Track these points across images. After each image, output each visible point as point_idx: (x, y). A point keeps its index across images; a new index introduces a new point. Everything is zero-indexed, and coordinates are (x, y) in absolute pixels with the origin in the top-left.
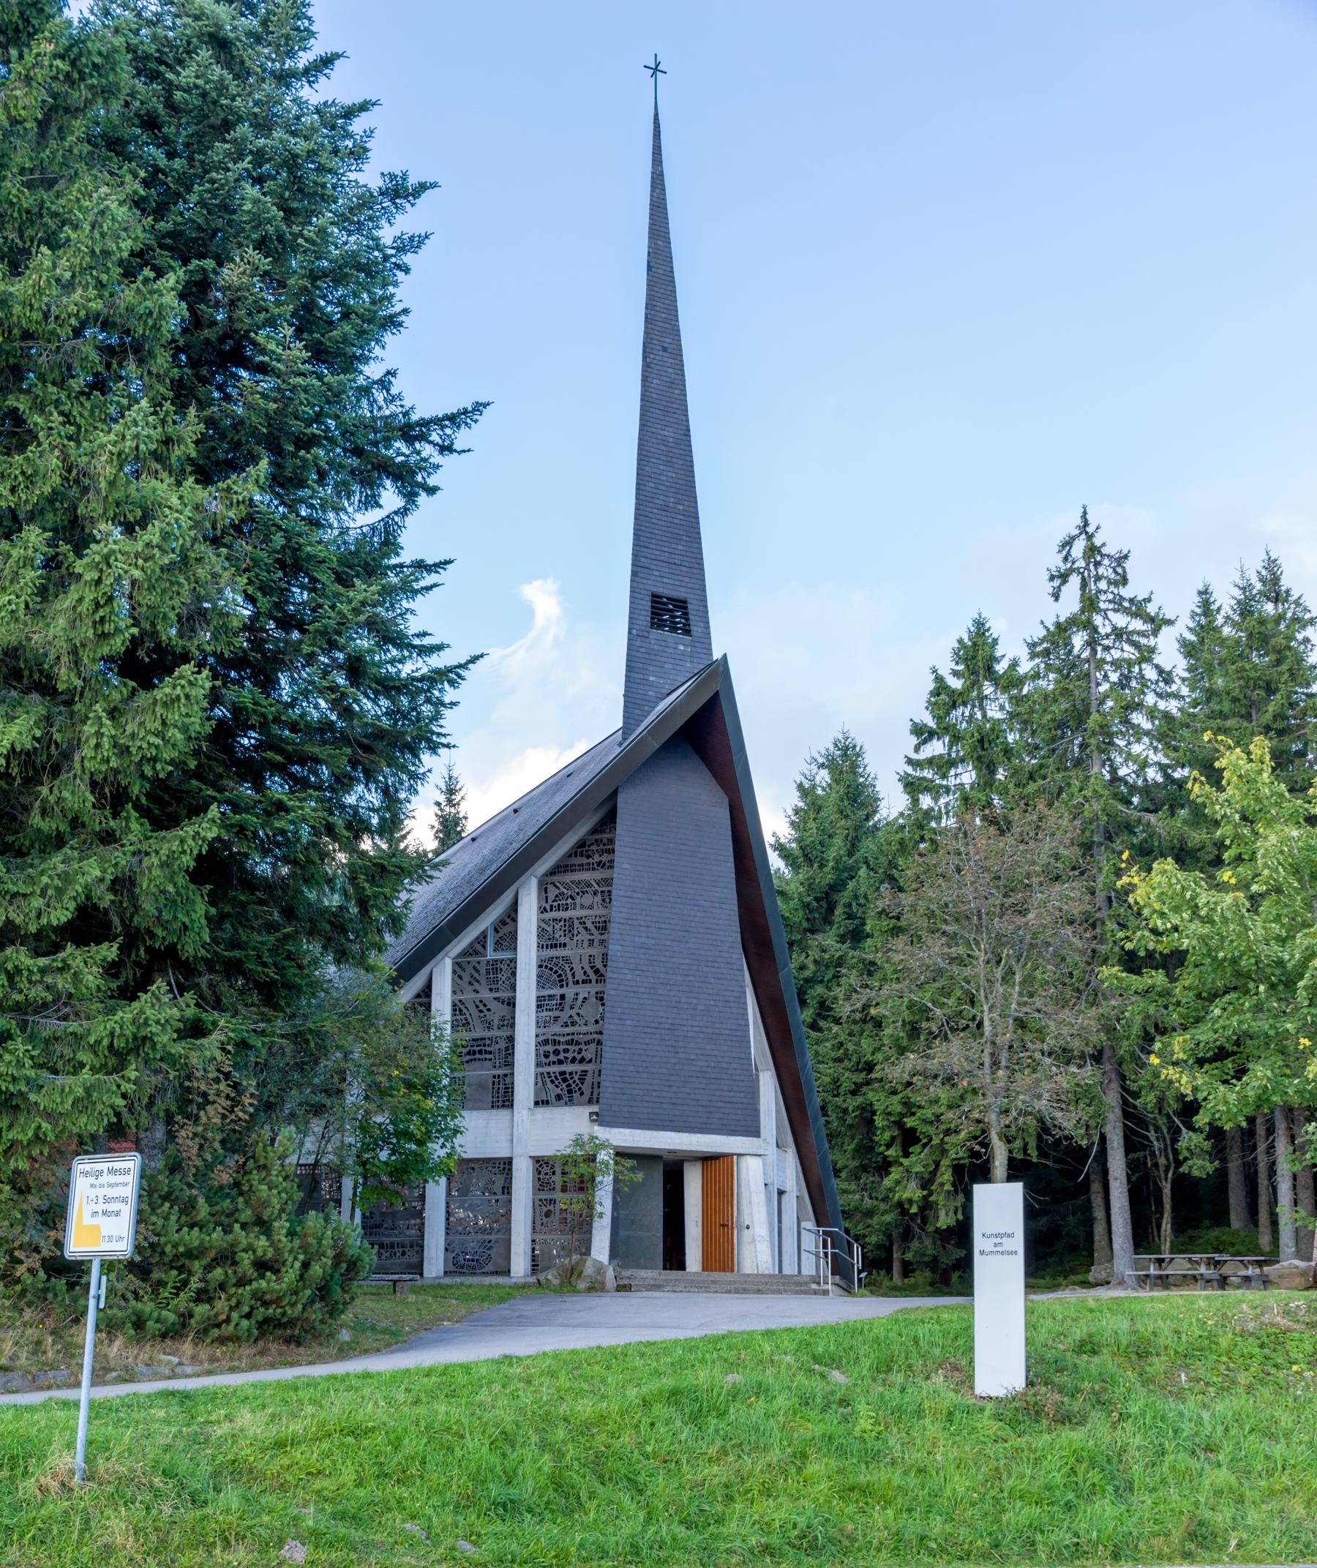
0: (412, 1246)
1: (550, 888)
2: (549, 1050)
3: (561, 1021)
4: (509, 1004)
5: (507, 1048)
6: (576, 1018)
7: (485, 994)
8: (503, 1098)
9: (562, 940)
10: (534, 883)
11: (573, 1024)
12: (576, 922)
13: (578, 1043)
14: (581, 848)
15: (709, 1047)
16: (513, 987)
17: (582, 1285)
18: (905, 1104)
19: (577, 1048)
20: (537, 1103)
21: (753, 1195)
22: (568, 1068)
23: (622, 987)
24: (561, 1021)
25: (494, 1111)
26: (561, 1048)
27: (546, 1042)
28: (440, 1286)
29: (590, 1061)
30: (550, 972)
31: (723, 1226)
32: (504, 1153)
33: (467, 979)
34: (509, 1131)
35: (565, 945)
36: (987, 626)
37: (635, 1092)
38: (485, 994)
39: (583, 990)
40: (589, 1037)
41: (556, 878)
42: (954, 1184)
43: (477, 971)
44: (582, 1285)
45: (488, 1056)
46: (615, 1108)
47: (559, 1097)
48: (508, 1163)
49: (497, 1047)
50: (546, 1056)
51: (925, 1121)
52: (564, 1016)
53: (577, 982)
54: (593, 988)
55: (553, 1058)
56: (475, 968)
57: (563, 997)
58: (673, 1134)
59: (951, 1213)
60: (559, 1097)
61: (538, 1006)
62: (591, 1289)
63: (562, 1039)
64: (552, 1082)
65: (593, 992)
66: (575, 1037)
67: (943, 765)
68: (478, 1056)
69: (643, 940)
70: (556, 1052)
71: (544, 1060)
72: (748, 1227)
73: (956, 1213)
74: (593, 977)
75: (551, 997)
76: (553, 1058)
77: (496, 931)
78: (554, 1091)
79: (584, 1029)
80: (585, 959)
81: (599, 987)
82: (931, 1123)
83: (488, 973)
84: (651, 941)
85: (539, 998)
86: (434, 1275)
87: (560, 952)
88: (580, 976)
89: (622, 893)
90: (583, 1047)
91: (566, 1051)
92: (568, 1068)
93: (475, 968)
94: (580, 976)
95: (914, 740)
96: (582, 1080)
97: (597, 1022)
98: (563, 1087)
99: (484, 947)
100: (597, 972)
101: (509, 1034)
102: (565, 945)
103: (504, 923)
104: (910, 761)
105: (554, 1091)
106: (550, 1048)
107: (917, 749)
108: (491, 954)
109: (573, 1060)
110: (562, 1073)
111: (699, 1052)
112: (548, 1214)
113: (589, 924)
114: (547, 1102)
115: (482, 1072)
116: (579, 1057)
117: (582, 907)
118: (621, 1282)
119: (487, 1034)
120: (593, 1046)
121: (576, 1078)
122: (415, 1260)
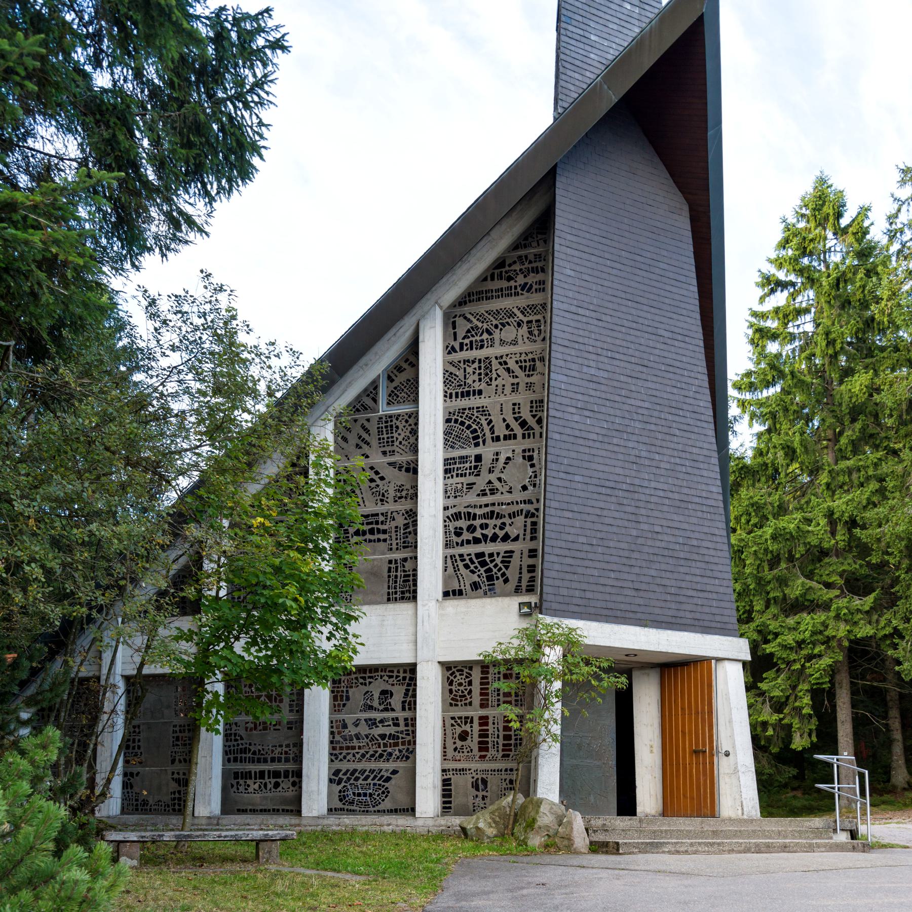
0: (286, 776)
1: (460, 321)
2: (460, 526)
3: (477, 489)
4: (407, 470)
5: (406, 526)
6: (497, 484)
7: (377, 459)
8: (404, 588)
9: (477, 386)
10: (439, 314)
11: (493, 492)
12: (495, 363)
13: (499, 516)
14: (499, 268)
15: (675, 517)
16: (415, 450)
17: (536, 841)
18: (759, 632)
19: (499, 522)
20: (446, 594)
21: (734, 711)
22: (487, 548)
23: (568, 431)
24: (477, 489)
25: (391, 606)
26: (477, 523)
27: (457, 516)
28: (327, 836)
29: (517, 538)
30: (460, 428)
31: (696, 752)
32: (407, 659)
33: (353, 439)
34: (411, 630)
35: (480, 392)
36: (830, 182)
37: (589, 572)
38: (377, 459)
39: (505, 449)
40: (515, 508)
41: (466, 309)
42: (813, 707)
43: (367, 431)
44: (536, 841)
45: (382, 536)
46: (564, 592)
47: (475, 586)
48: (411, 669)
49: (393, 524)
50: (458, 533)
51: (785, 647)
52: (481, 482)
53: (498, 439)
54: (519, 445)
55: (466, 536)
56: (363, 427)
57: (478, 458)
58: (638, 629)
59: (806, 735)
60: (475, 586)
61: (446, 471)
62: (550, 847)
63: (479, 512)
64: (466, 566)
65: (519, 450)
66: (497, 509)
67: (786, 315)
68: (368, 536)
69: (593, 371)
70: (471, 529)
71: (455, 538)
72: (727, 754)
73: (810, 735)
74: (519, 431)
75: (464, 459)
76: (466, 536)
77: (390, 379)
78: (469, 578)
79: (507, 498)
80: (508, 409)
81: (528, 444)
82: (791, 649)
83: (380, 432)
84: (602, 374)
85: (446, 461)
86: (315, 814)
87: (474, 402)
88: (501, 431)
89: (565, 307)
90: (507, 520)
91: (484, 526)
92: (487, 548)
93: (363, 427)
94: (501, 431)
95: (760, 292)
96: (506, 563)
97: (524, 488)
98: (476, 574)
99: (375, 401)
100: (523, 424)
101: (408, 507)
102: (480, 392)
103: (399, 369)
104: (755, 314)
105: (469, 578)
106: (463, 524)
107: (762, 300)
108: (383, 409)
109: (494, 538)
110: (480, 555)
111: (664, 523)
112: (463, 736)
113: (511, 364)
114: (460, 593)
115: (371, 557)
116: (501, 534)
117: (502, 342)
118: (600, 837)
119: (380, 509)
120: (520, 520)
121: (498, 560)
122: (290, 793)
